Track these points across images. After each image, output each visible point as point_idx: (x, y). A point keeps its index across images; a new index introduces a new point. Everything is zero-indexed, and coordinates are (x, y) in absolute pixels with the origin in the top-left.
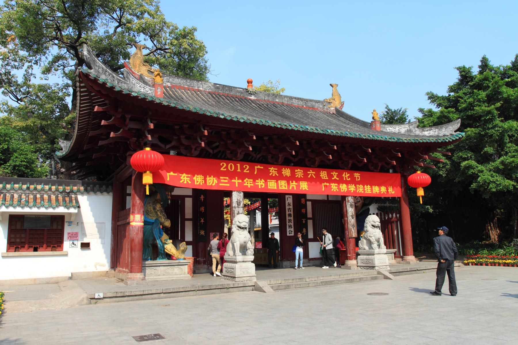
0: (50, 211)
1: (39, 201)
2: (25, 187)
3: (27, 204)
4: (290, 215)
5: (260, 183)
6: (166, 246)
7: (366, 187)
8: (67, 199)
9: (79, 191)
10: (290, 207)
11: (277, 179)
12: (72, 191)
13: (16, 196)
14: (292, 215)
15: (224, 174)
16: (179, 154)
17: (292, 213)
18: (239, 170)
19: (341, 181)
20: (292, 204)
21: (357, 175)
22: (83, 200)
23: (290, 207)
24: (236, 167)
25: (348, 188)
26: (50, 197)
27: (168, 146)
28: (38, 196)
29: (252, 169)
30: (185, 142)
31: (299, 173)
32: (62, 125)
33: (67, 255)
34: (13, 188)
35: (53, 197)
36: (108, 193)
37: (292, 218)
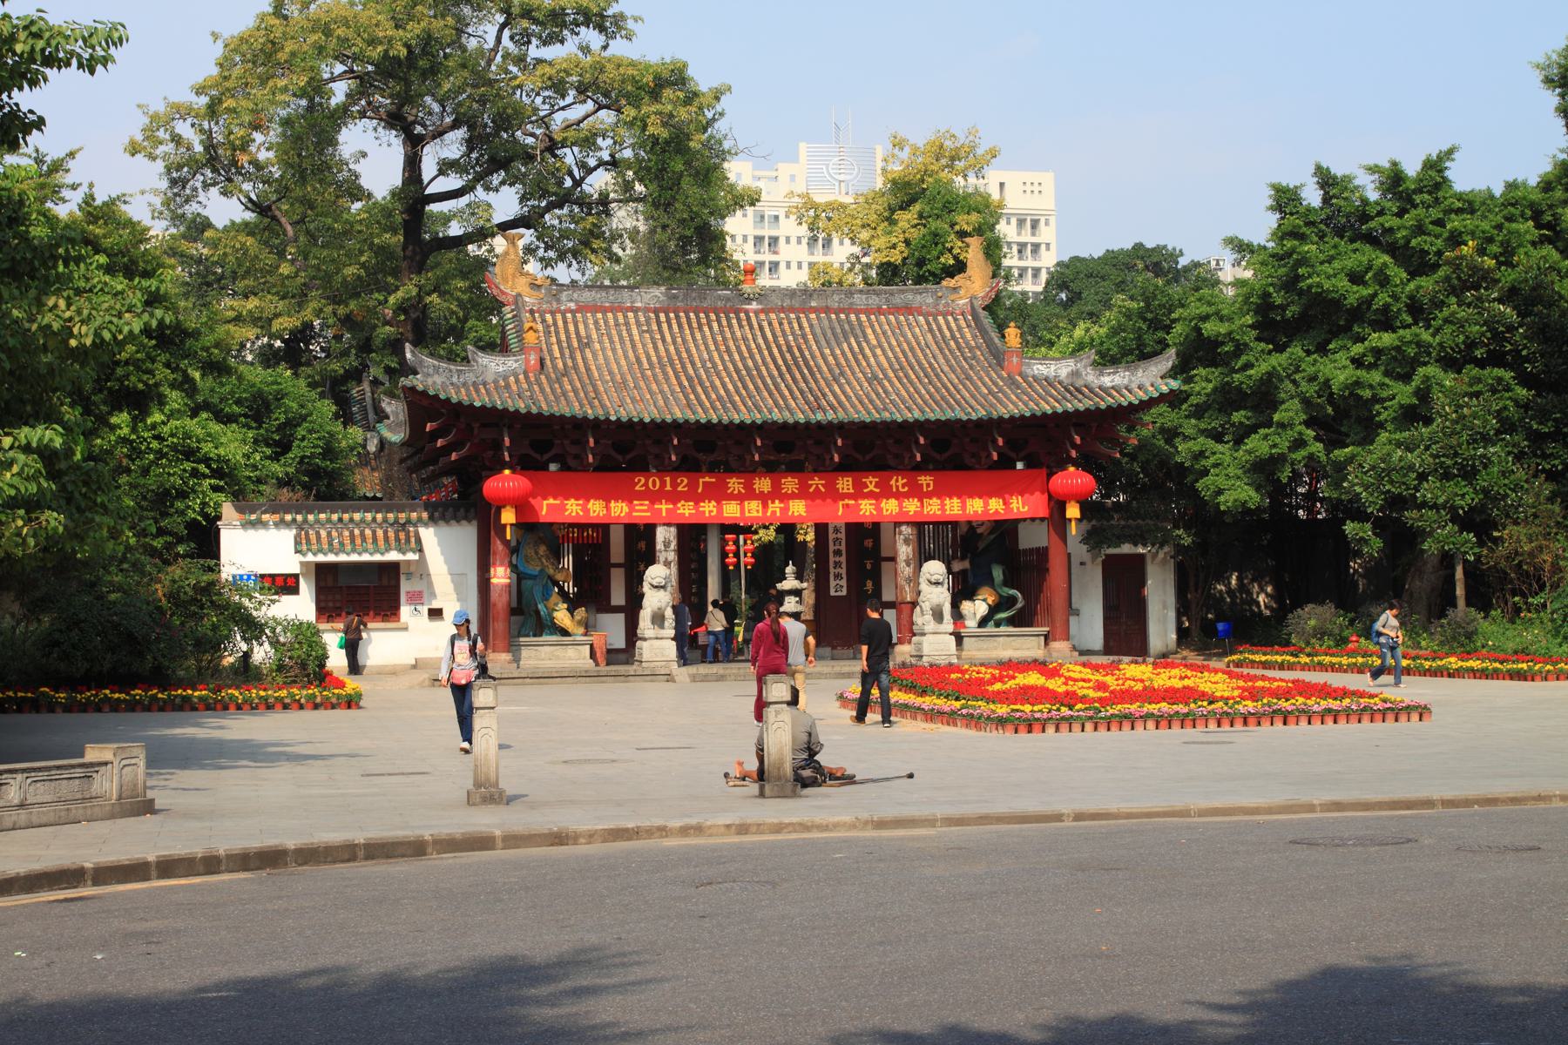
0: (378, 558)
1: (358, 541)
2: (335, 517)
3: (342, 549)
4: (838, 553)
5: (709, 508)
6: (556, 614)
7: (947, 501)
8: (402, 535)
9: (420, 520)
11: (741, 498)
12: (409, 522)
13: (323, 534)
16: (565, 468)
17: (843, 548)
18: (668, 488)
19: (886, 492)
21: (926, 480)
22: (429, 536)
24: (663, 484)
25: (891, 506)
26: (374, 533)
27: (546, 457)
28: (357, 532)
29: (693, 485)
31: (790, 484)
32: (384, 316)
33: (406, 629)
34: (317, 521)
35: (380, 533)
36: (469, 521)
37: (843, 559)
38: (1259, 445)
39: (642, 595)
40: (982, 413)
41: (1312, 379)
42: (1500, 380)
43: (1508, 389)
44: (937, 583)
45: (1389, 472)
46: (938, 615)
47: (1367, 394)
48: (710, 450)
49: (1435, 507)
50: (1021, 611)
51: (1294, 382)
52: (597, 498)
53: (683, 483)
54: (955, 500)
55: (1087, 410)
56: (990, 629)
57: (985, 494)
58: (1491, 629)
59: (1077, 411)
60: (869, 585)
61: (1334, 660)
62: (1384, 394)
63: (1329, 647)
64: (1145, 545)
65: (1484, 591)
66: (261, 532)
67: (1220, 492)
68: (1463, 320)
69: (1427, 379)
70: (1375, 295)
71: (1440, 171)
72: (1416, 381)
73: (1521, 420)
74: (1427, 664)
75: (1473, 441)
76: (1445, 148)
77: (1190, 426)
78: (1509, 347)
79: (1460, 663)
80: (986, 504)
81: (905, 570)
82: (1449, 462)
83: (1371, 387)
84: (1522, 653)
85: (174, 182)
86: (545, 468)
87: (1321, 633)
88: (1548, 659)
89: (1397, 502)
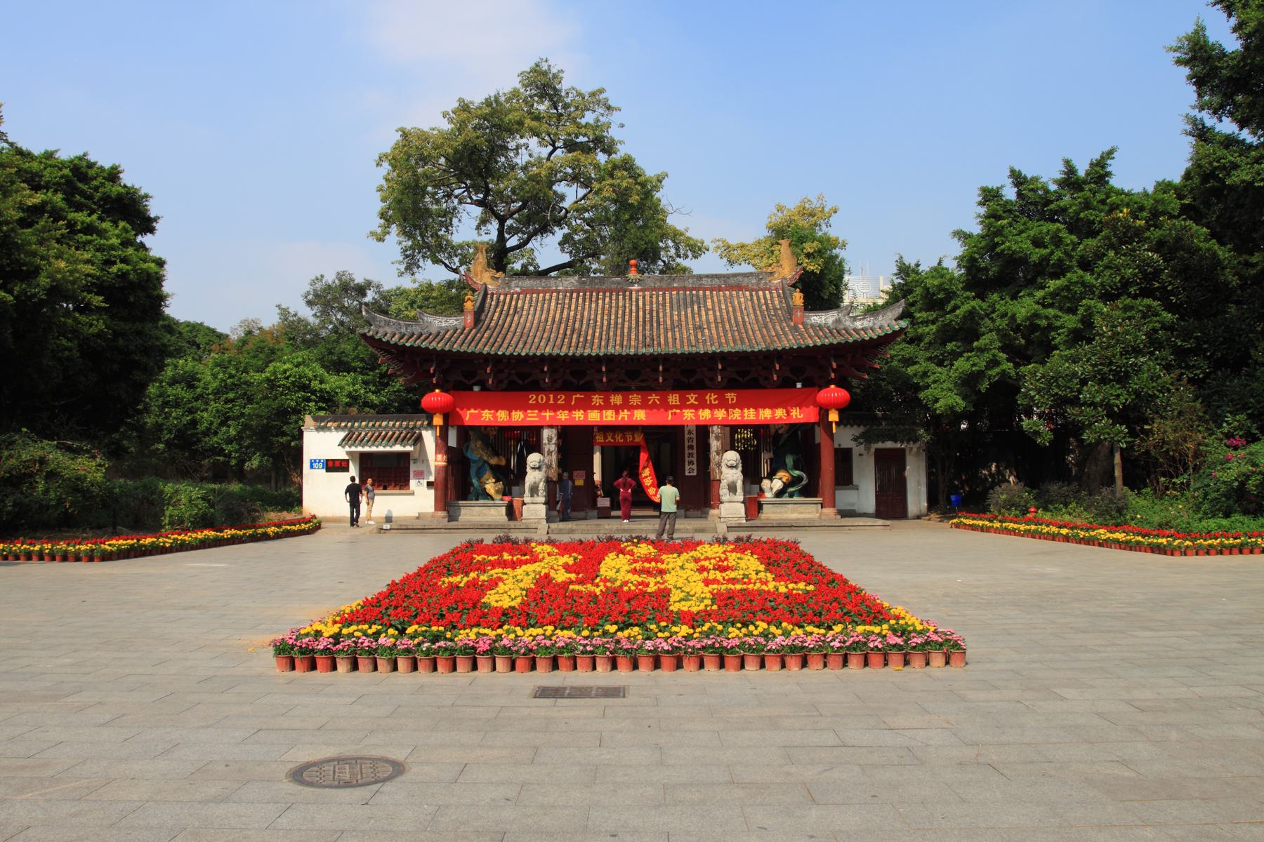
5: (578, 416)
11: (600, 408)
12: (415, 427)
15: (532, 407)
17: (694, 444)
19: (703, 405)
21: (731, 396)
24: (548, 399)
29: (568, 400)
31: (635, 399)
37: (694, 451)
38: (962, 365)
39: (526, 473)
40: (763, 347)
41: (1004, 315)
42: (1149, 307)
43: (1157, 315)
44: (732, 467)
45: (1056, 379)
46: (732, 488)
47: (1044, 323)
48: (576, 375)
49: (1093, 404)
50: (805, 487)
51: (993, 320)
52: (502, 409)
53: (562, 399)
54: (752, 410)
55: (839, 344)
56: (785, 499)
57: (773, 407)
58: (1141, 504)
59: (831, 344)
61: (1016, 526)
62: (1058, 324)
63: (1016, 516)
64: (902, 442)
65: (1141, 473)
66: (328, 433)
67: (937, 400)
68: (1120, 265)
69: (1089, 308)
70: (1052, 253)
71: (1103, 167)
72: (1081, 311)
73: (1168, 339)
74: (1082, 534)
75: (1124, 353)
76: (1106, 149)
77: (922, 354)
78: (1157, 285)
79: (1109, 535)
80: (773, 413)
82: (1106, 369)
83: (1047, 318)
84: (1162, 528)
85: (407, 256)
86: (472, 389)
87: (1009, 505)
88: (1188, 534)
89: (1061, 402)
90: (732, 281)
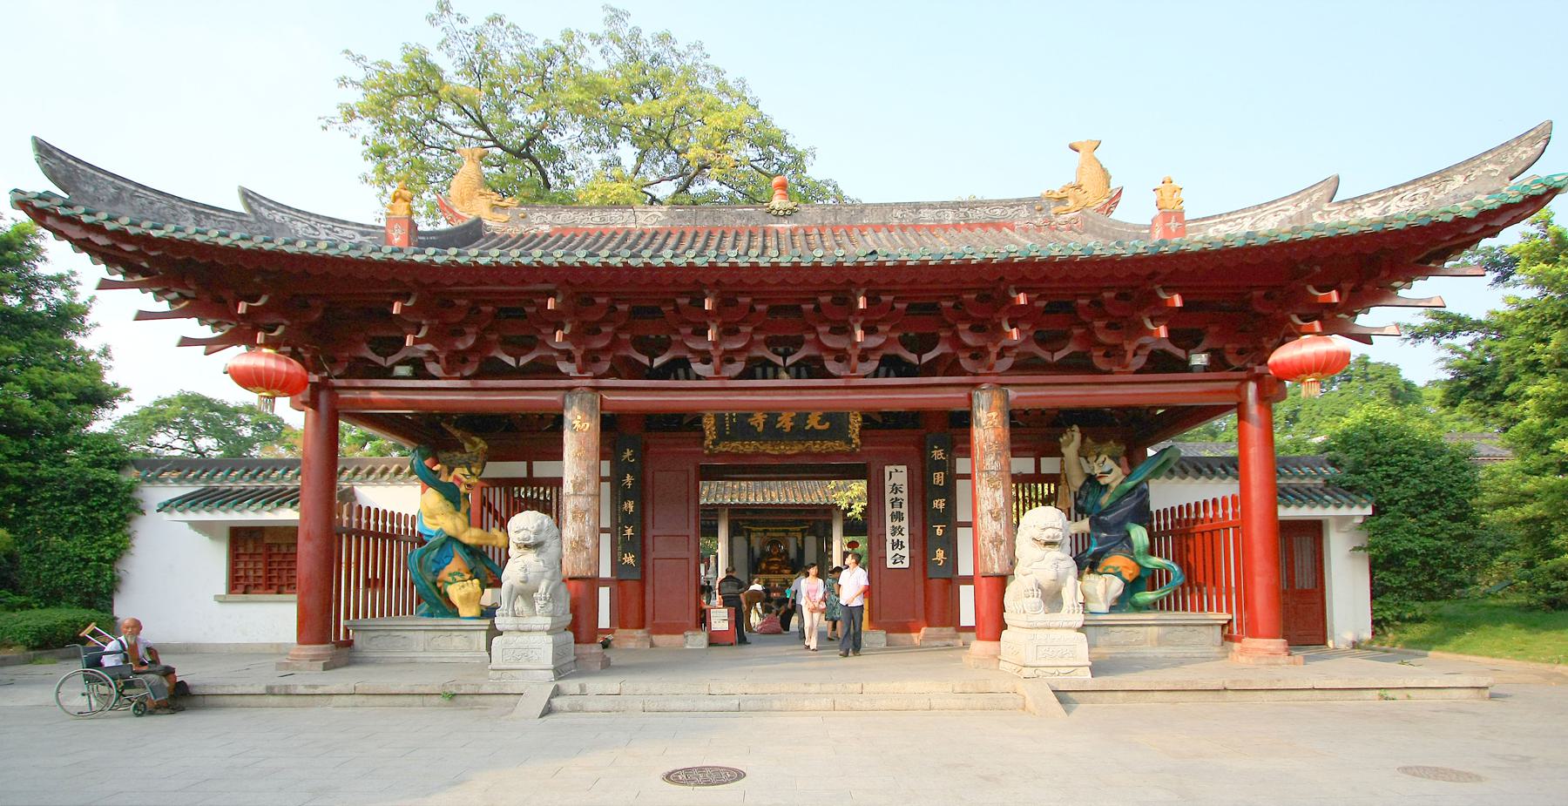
10: (899, 495)
14: (906, 516)
17: (905, 510)
20: (905, 489)
23: (899, 495)
27: (391, 360)
30: (968, 339)
37: (905, 524)
60: (940, 555)
81: (990, 527)
90: (978, 215)
